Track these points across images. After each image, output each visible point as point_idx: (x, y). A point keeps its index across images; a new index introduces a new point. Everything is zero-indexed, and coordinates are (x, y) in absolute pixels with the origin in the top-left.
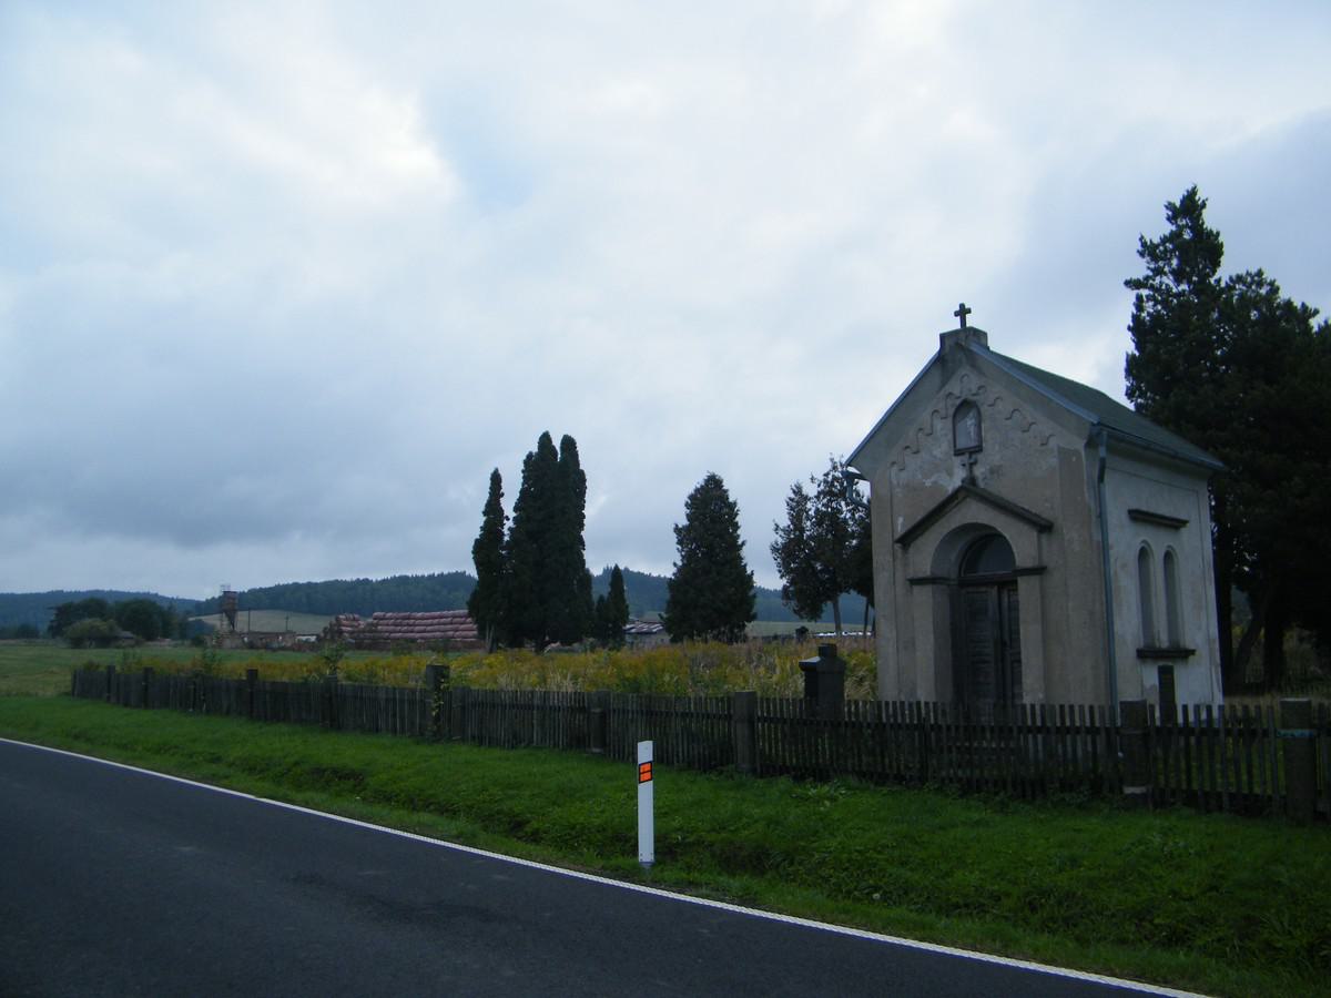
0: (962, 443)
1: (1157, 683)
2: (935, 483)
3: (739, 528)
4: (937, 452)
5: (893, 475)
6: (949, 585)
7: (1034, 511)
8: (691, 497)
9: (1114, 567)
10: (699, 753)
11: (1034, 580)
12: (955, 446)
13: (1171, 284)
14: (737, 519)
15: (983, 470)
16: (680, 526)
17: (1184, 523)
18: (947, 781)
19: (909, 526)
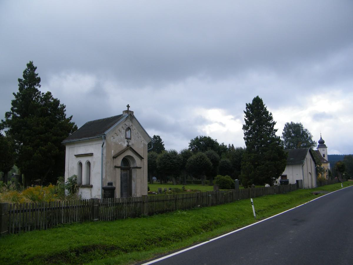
2: (121, 144)
10: (132, 213)
12: (126, 136)
15: (131, 144)
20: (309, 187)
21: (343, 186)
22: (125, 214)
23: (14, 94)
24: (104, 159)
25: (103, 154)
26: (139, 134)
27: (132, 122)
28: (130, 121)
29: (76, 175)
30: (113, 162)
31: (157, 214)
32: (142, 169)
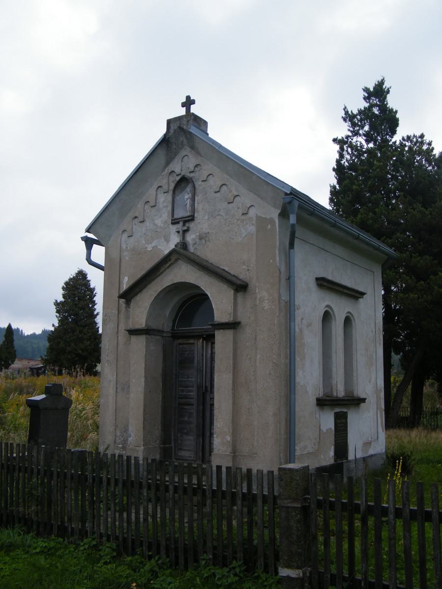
0: (180, 213)
1: (333, 428)
3: (96, 304)
4: (159, 222)
5: (123, 239)
6: (163, 337)
7: (232, 273)
8: (66, 283)
9: (299, 323)
11: (229, 333)
13: (364, 143)
14: (95, 299)
15: (193, 236)
16: (59, 301)
17: (363, 294)
18: (104, 539)
19: (132, 282)
20: (181, 449)
21: (176, 485)
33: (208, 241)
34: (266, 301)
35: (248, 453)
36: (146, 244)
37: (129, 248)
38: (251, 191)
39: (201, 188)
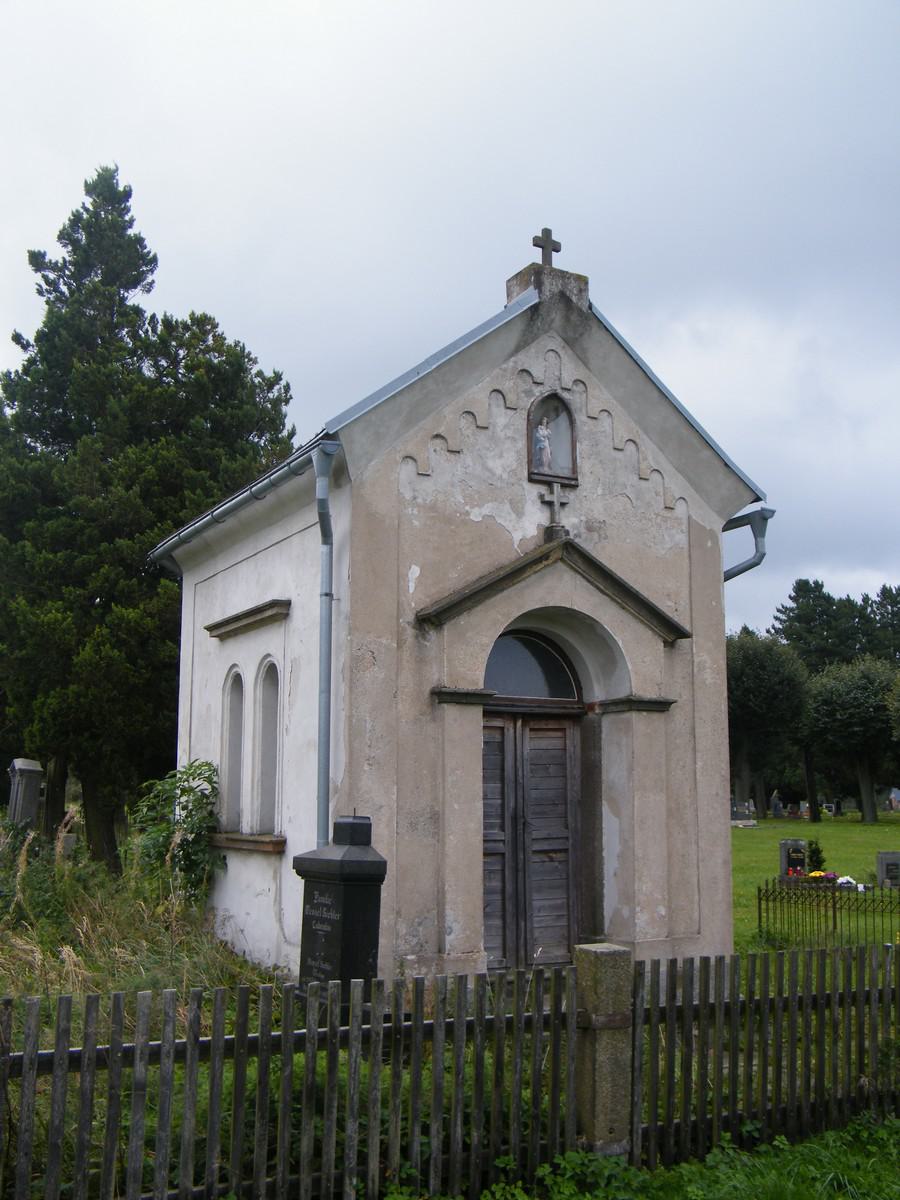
4: (496, 465)
15: (575, 520)
22: (363, 1158)
23: (17, 338)
24: (340, 634)
25: (329, 595)
26: (648, 446)
27: (583, 359)
28: (567, 356)
29: (216, 763)
30: (421, 661)
31: (745, 1143)
32: (678, 714)
33: (605, 539)
34: (708, 670)
35: (684, 933)
36: (466, 504)
37: (419, 500)
38: (679, 472)
39: (586, 428)
